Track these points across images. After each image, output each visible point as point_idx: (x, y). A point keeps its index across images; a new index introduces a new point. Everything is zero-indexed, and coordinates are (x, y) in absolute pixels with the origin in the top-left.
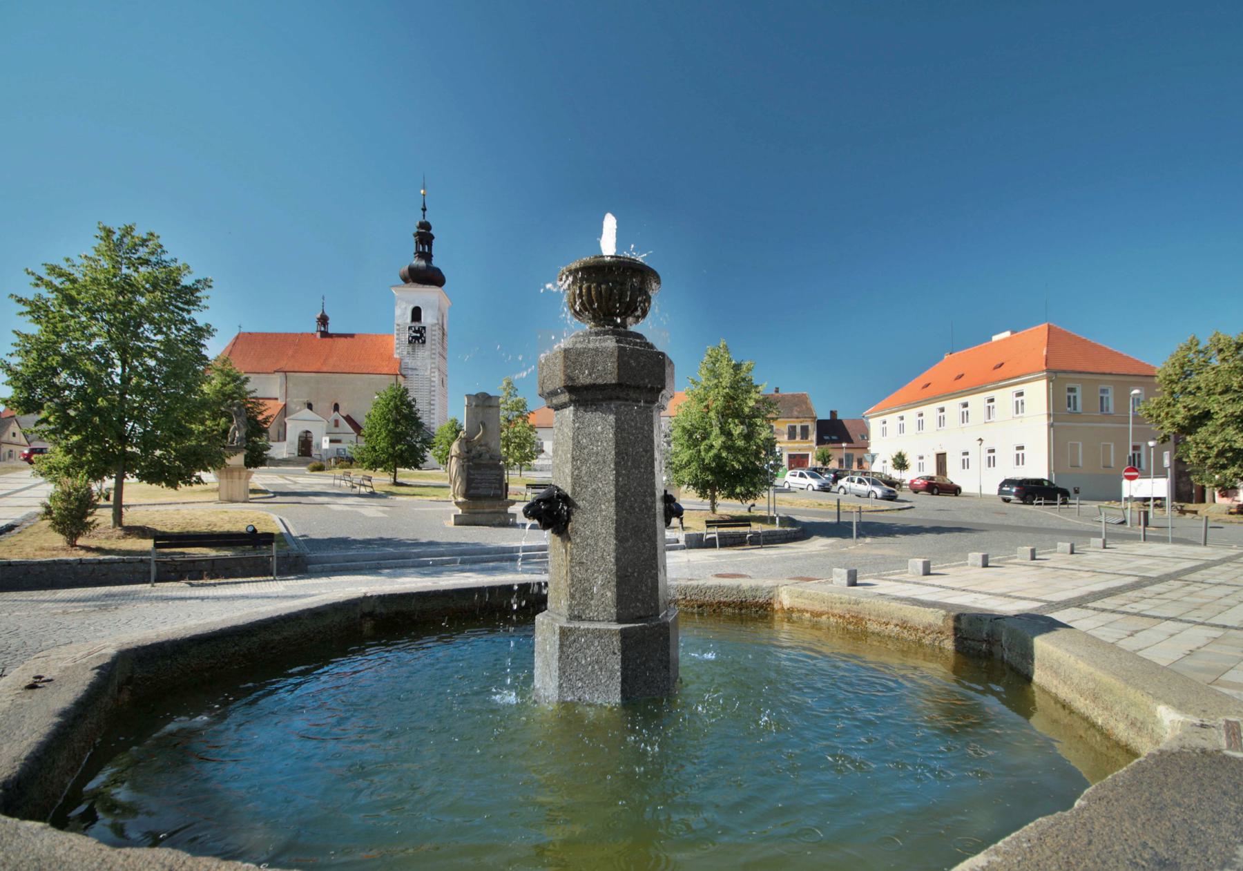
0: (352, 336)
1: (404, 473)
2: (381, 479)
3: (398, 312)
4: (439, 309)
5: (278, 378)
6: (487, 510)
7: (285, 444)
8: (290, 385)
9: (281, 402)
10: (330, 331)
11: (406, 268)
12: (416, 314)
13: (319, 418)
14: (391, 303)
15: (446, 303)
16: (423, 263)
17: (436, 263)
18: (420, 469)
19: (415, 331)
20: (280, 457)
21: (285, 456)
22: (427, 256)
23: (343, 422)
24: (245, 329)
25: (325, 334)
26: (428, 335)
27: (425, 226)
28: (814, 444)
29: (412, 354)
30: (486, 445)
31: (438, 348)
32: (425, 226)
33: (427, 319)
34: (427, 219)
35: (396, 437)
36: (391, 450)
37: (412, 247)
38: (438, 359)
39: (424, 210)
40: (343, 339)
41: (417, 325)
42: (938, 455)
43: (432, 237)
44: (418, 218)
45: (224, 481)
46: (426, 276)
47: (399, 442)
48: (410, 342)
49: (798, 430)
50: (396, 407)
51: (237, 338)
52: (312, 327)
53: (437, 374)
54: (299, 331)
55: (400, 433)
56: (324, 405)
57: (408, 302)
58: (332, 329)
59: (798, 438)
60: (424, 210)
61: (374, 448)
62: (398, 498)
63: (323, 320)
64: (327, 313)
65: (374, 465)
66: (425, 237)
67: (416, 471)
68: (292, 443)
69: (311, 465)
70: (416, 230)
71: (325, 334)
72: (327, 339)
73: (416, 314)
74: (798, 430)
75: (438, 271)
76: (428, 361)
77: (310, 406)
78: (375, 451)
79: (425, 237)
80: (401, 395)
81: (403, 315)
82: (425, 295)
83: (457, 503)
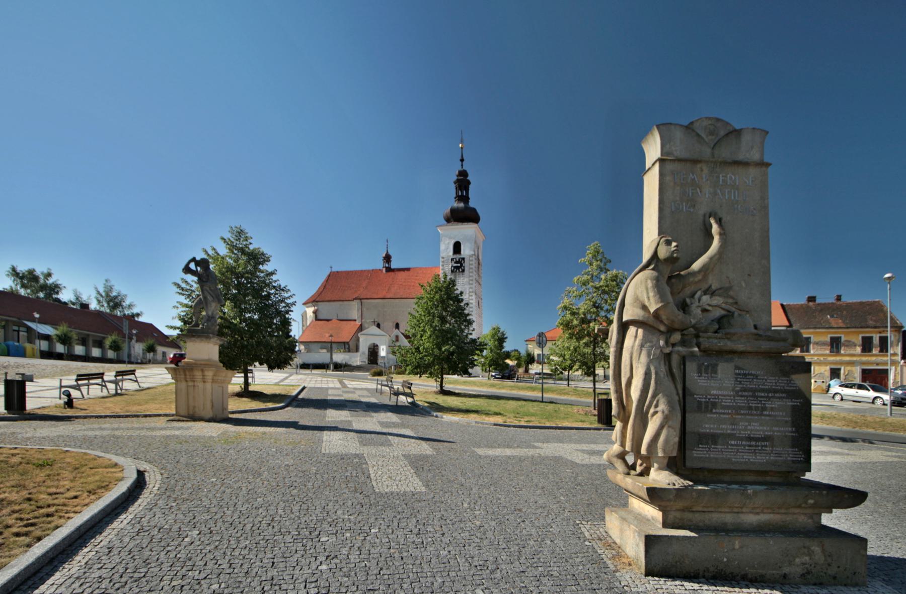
0: (408, 269)
1: (453, 381)
2: (424, 387)
3: (442, 247)
4: (475, 242)
5: (355, 304)
6: (751, 519)
7: (359, 354)
8: (364, 309)
9: (358, 323)
10: (393, 267)
11: (449, 210)
12: (457, 247)
13: (383, 333)
14: (437, 240)
15: (481, 238)
16: (462, 205)
17: (472, 204)
18: (470, 375)
19: (456, 262)
20: (355, 364)
21: (359, 363)
22: (464, 198)
23: (402, 337)
24: (334, 270)
25: (389, 270)
26: (466, 264)
27: (463, 174)
28: (899, 358)
30: (724, 291)
31: (475, 276)
32: (463, 174)
33: (466, 251)
34: (465, 168)
35: (443, 336)
36: (436, 351)
37: (453, 193)
38: (475, 284)
39: (462, 160)
41: (457, 257)
42: (8, 384)
43: (469, 183)
44: (458, 168)
45: (183, 385)
46: (463, 215)
47: (445, 342)
48: (452, 271)
49: (876, 341)
50: (442, 301)
51: (329, 276)
52: (380, 265)
53: (474, 297)
54: (371, 268)
55: (448, 331)
56: (390, 325)
57: (450, 238)
58: (394, 265)
59: (875, 351)
60: (462, 160)
61: (417, 349)
62: (448, 417)
63: (388, 258)
64: (390, 253)
65: (420, 369)
66: (463, 183)
67: (465, 378)
68: (363, 353)
69: (373, 370)
70: (456, 178)
71: (389, 270)
72: (390, 273)
73: (457, 247)
74: (876, 341)
75: (474, 210)
76: (467, 287)
77: (378, 326)
78: (419, 352)
79: (463, 183)
80: (447, 288)
81: (446, 249)
82: (465, 231)
83: (654, 495)
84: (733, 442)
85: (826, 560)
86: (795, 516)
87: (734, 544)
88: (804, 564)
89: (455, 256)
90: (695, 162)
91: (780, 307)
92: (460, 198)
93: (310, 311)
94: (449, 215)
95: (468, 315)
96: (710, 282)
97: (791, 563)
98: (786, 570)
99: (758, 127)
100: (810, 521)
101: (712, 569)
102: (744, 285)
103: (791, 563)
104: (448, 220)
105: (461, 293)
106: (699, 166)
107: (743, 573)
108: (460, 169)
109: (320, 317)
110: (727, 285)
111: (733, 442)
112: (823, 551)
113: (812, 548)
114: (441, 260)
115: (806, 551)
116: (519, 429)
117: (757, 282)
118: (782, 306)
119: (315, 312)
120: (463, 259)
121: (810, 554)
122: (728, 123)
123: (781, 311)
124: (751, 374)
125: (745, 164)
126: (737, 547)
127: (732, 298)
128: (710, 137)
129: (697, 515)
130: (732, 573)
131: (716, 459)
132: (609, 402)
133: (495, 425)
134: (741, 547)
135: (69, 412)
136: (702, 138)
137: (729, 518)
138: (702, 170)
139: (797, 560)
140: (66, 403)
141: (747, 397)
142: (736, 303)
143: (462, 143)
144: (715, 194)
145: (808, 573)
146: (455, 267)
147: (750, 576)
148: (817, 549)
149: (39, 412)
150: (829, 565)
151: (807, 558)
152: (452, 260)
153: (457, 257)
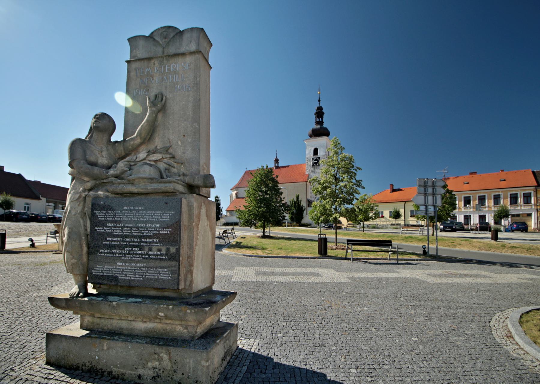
0: (288, 166)
2: (250, 234)
3: (307, 152)
6: (141, 326)
10: (279, 166)
12: (316, 151)
14: (304, 148)
16: (319, 126)
17: (325, 125)
22: (321, 123)
24: (248, 170)
25: (277, 167)
27: (320, 109)
29: (314, 171)
32: (320, 109)
33: (321, 153)
34: (321, 105)
39: (319, 101)
40: (284, 168)
41: (316, 157)
43: (323, 113)
46: (320, 132)
48: (313, 166)
57: (312, 146)
58: (280, 165)
60: (319, 101)
63: (277, 161)
64: (278, 158)
66: (320, 113)
71: (277, 167)
73: (316, 151)
75: (326, 129)
79: (320, 113)
81: (309, 153)
82: (321, 142)
84: (120, 264)
85: (172, 367)
86: (173, 326)
87: (103, 346)
88: (154, 368)
89: (314, 157)
90: (149, 59)
91: (531, 173)
92: (318, 123)
93: (234, 193)
94: (311, 133)
95: (280, 189)
96: (156, 144)
97: (144, 367)
98: (141, 371)
99: (195, 26)
100: (185, 331)
101: (88, 364)
102: (180, 143)
103: (144, 367)
104: (311, 136)
105: (277, 177)
106: (152, 61)
107: (109, 370)
108: (318, 106)
109: (239, 196)
110: (168, 145)
111: (120, 264)
112: (170, 358)
113: (161, 355)
114: (306, 159)
115: (156, 356)
116: (257, 258)
117: (189, 140)
118: (533, 172)
119: (236, 194)
120: (319, 158)
121: (160, 360)
122: (176, 28)
123: (532, 176)
124: (135, 210)
125: (183, 54)
126: (105, 348)
127: (170, 154)
128: (164, 40)
129: (103, 320)
130: (101, 369)
131: (108, 276)
132: (348, 241)
133: (244, 255)
134: (108, 349)
135: (33, 249)
136: (158, 42)
137: (124, 324)
138: (154, 64)
139: (150, 364)
140: (31, 245)
141: (131, 227)
142: (174, 157)
143: (319, 91)
144: (162, 79)
145: (158, 376)
146: (314, 163)
147: (114, 373)
148: (165, 356)
149: (14, 250)
150: (175, 371)
151: (157, 363)
152: (313, 159)
153: (316, 157)
